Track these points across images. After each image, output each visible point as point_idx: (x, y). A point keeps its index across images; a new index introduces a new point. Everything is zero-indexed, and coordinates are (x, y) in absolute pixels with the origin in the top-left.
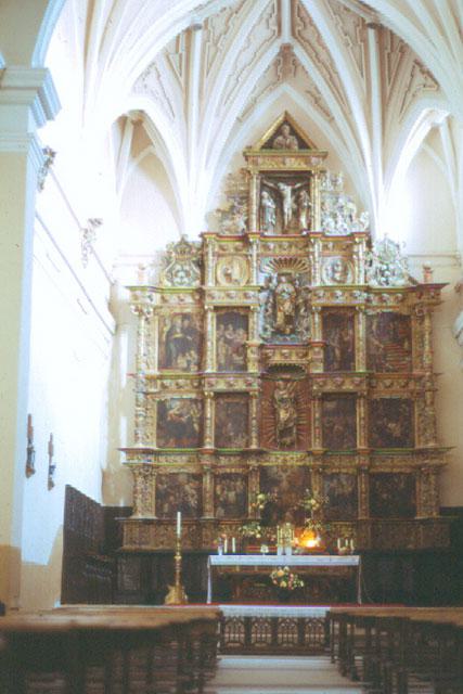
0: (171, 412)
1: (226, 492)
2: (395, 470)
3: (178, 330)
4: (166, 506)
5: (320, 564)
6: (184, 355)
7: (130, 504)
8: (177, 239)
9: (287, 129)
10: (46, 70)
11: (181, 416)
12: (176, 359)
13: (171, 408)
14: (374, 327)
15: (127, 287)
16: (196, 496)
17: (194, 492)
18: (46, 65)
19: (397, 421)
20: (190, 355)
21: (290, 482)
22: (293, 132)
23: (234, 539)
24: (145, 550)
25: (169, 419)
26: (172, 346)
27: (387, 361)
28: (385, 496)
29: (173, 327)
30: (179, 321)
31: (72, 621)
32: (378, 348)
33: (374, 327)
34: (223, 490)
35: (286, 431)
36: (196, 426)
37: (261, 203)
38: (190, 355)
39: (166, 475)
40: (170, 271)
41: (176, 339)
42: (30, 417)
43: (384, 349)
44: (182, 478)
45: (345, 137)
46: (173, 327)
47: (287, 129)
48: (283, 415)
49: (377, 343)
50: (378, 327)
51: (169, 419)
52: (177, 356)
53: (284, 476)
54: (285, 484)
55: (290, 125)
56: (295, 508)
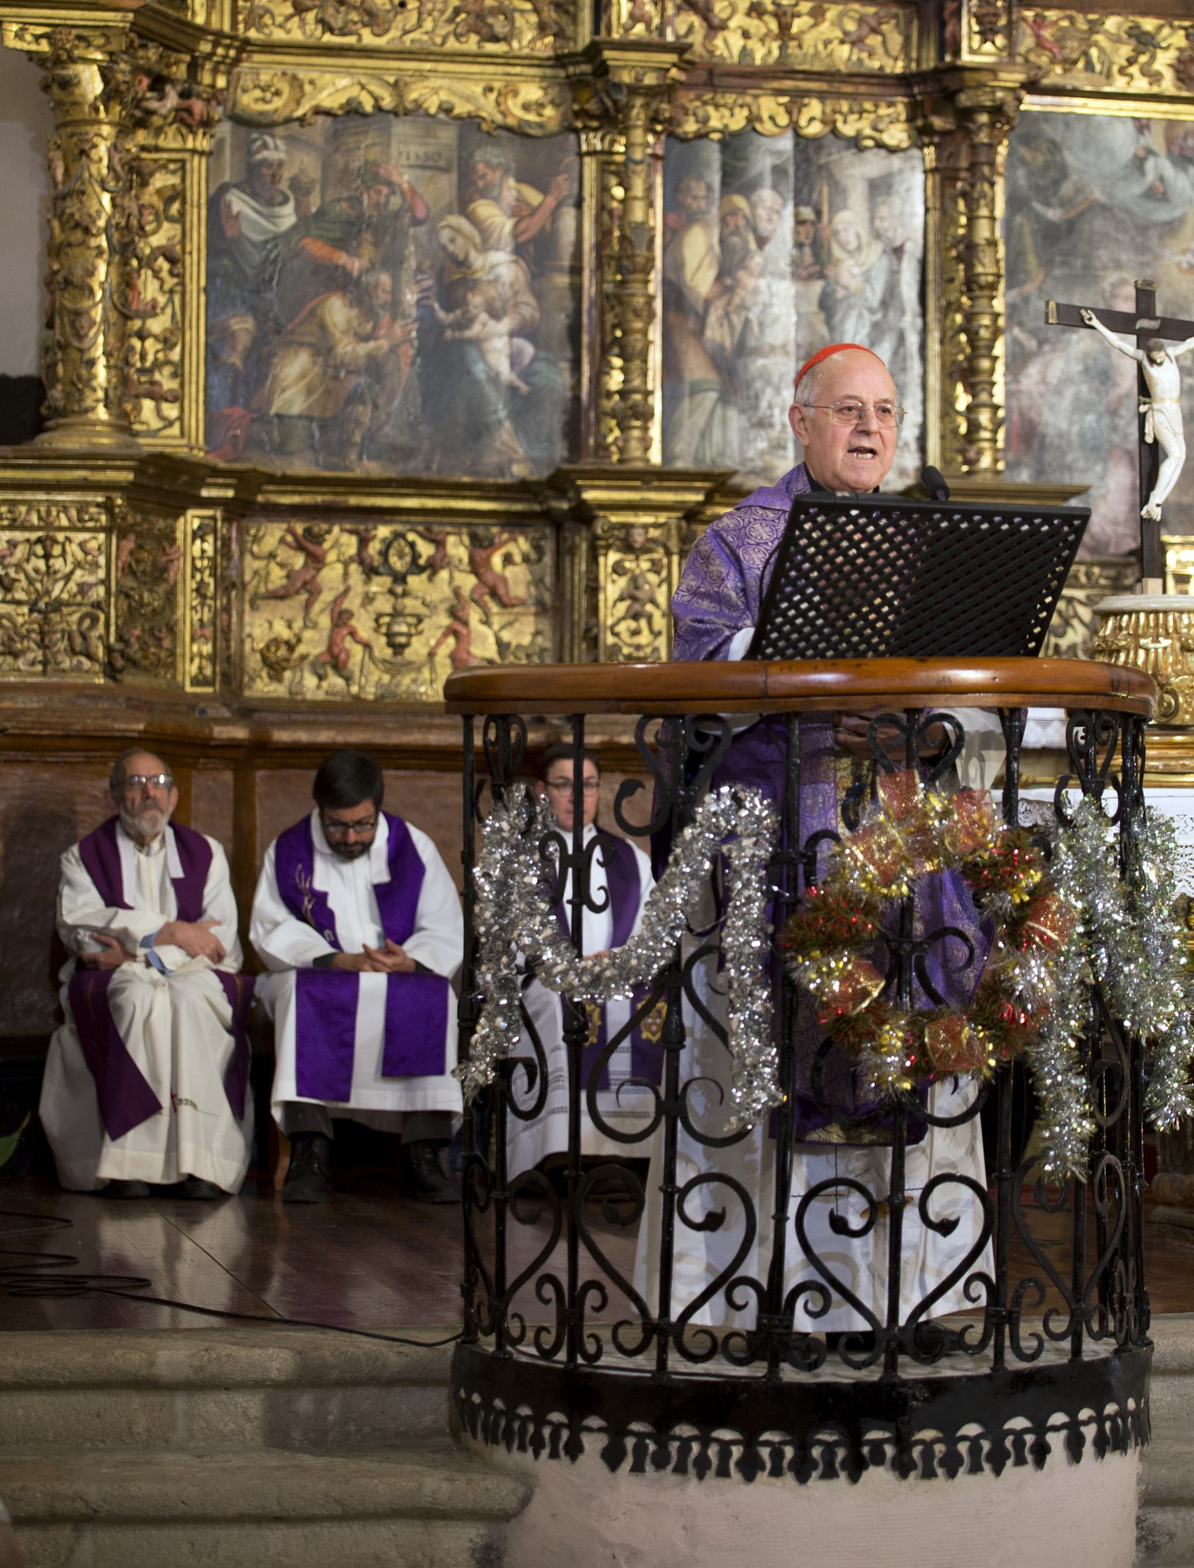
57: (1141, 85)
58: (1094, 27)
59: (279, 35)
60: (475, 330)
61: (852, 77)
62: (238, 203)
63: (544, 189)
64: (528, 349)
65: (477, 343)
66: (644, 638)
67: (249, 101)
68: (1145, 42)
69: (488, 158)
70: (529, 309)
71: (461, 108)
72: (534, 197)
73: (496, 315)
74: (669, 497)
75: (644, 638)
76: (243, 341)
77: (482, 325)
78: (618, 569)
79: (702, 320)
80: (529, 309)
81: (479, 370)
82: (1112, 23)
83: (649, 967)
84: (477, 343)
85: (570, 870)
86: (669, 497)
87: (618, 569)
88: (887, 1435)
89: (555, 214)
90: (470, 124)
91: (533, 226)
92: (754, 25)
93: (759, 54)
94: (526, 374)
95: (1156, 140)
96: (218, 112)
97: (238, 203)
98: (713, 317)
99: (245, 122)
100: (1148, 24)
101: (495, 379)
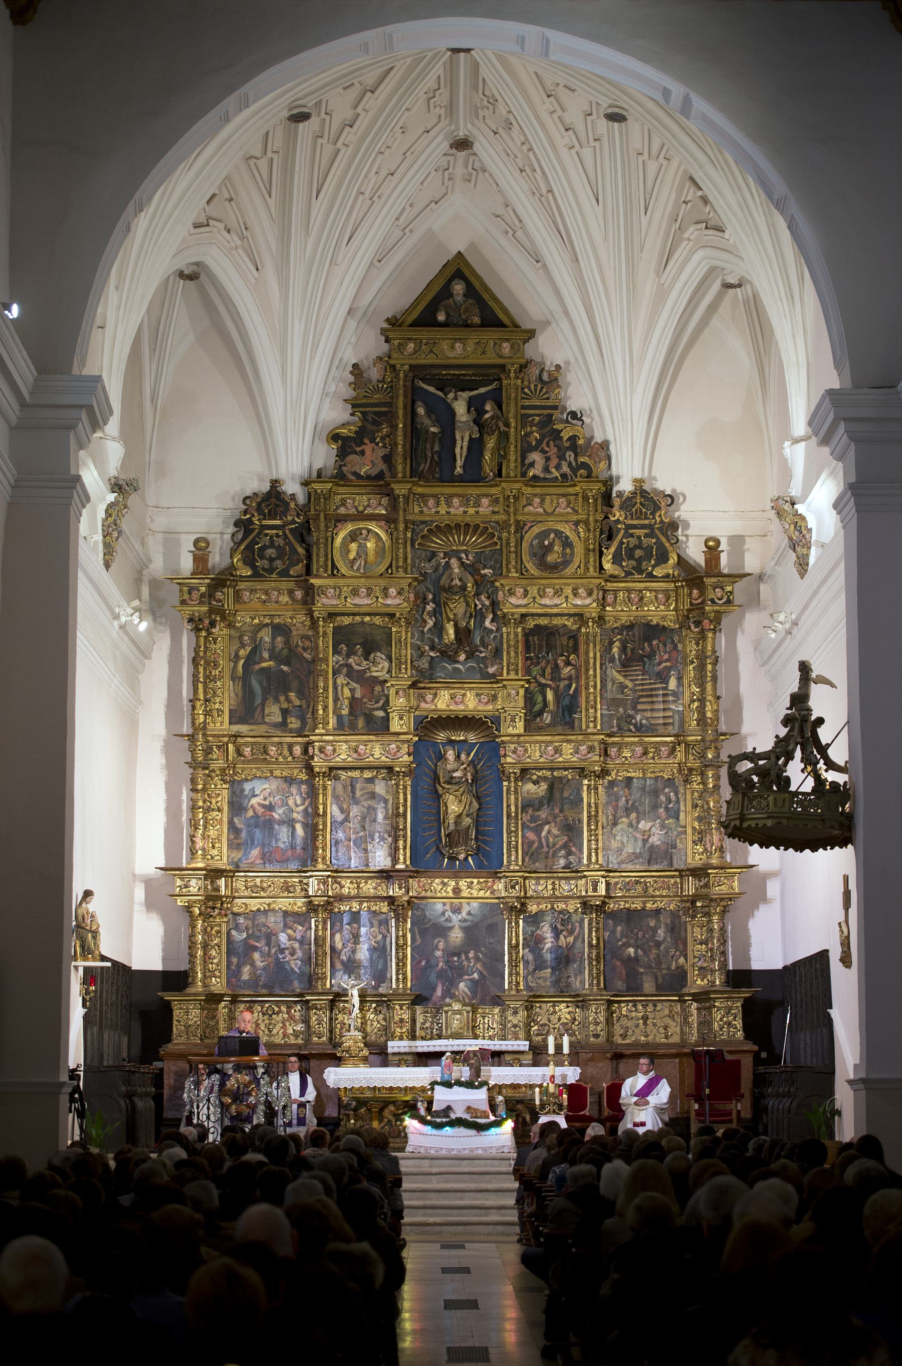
3: (266, 655)
4: (246, 969)
5: (845, 1056)
7: (183, 967)
9: (458, 288)
10: (80, 476)
12: (263, 705)
16: (299, 954)
18: (81, 473)
21: (466, 930)
22: (471, 292)
23: (506, 987)
24: (528, 1324)
27: (638, 711)
28: (631, 950)
30: (266, 636)
38: (288, 700)
39: (245, 915)
40: (249, 547)
42: (445, 1271)
44: (273, 921)
45: (568, 300)
47: (458, 288)
48: (454, 806)
52: (264, 700)
53: (455, 918)
56: (476, 975)
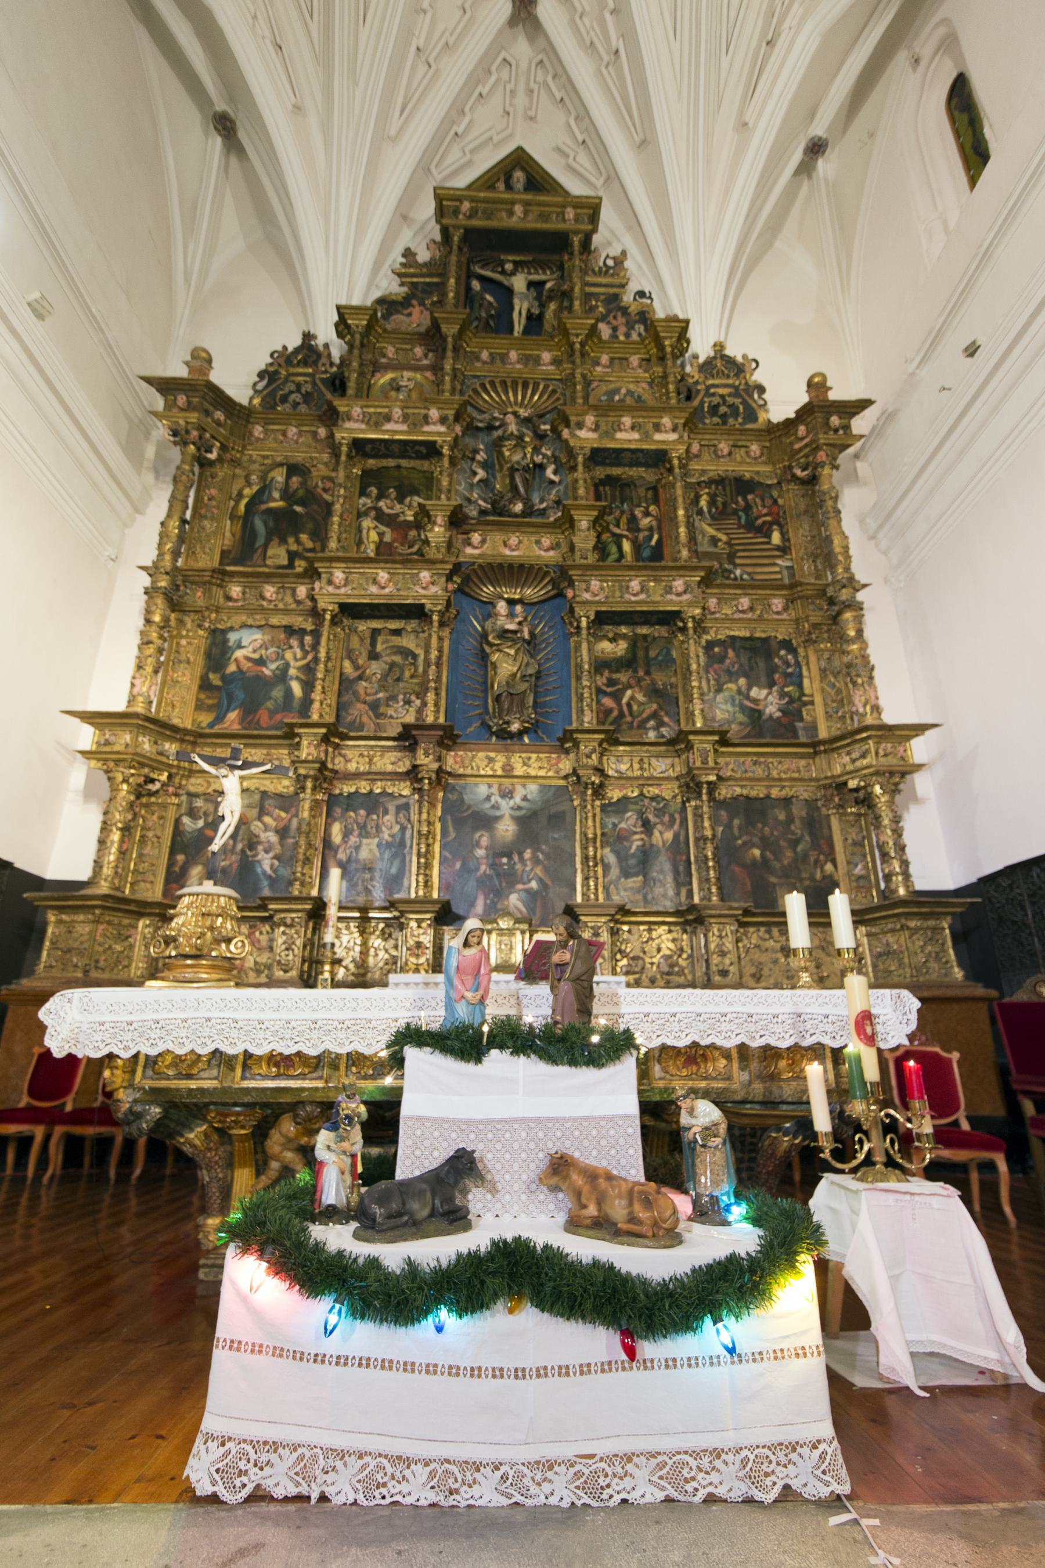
0: (239, 654)
1: (353, 839)
2: (775, 793)
3: (276, 495)
6: (283, 541)
8: (294, 342)
11: (261, 662)
12: (265, 547)
13: (240, 646)
14: (703, 503)
15: (149, 380)
17: (273, 838)
19: (771, 684)
20: (298, 541)
25: (232, 668)
26: (259, 524)
29: (265, 489)
30: (279, 476)
31: (937, 1157)
32: (714, 541)
33: (703, 503)
34: (346, 834)
35: (502, 700)
36: (297, 688)
37: (587, 1227)
38: (298, 541)
41: (270, 511)
43: (729, 543)
46: (265, 489)
49: (711, 531)
50: (712, 502)
51: (232, 668)
53: (506, 806)
54: (507, 829)
55: (523, 169)
57: (490, 773)
58: (473, 757)
59: (482, 772)
60: (259, 857)
61: (390, 773)
62: (186, 820)
63: (287, 812)
64: (276, 863)
65: (259, 862)
66: (291, 957)
67: (192, 789)
68: (491, 760)
69: (269, 803)
70: (278, 849)
71: (262, 789)
72: (283, 814)
73: (267, 851)
74: (299, 907)
75: (291, 957)
76: (180, 863)
77: (262, 855)
78: (284, 933)
79: (336, 852)
80: (278, 849)
81: (259, 870)
82: (481, 755)
83: (917, 930)
84: (259, 862)
85: (979, 900)
86: (299, 907)
87: (284, 933)
88: (318, 1232)
89: (290, 820)
90: (264, 794)
91: (282, 824)
92: (361, 760)
93: (362, 769)
94: (275, 871)
95: (495, 790)
96: (181, 792)
97: (186, 820)
98: (340, 851)
99: (190, 795)
100: (492, 755)
101: (264, 873)
